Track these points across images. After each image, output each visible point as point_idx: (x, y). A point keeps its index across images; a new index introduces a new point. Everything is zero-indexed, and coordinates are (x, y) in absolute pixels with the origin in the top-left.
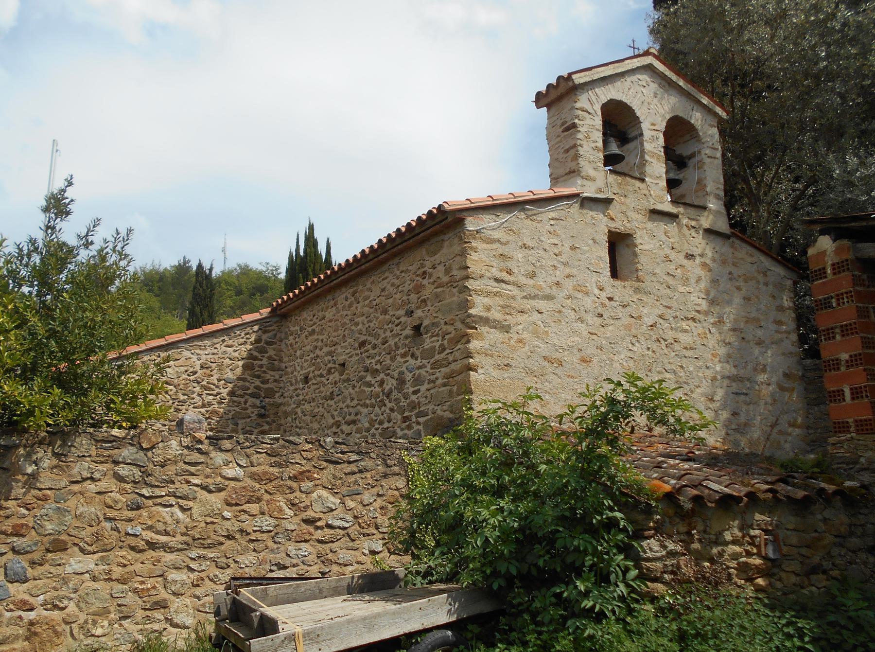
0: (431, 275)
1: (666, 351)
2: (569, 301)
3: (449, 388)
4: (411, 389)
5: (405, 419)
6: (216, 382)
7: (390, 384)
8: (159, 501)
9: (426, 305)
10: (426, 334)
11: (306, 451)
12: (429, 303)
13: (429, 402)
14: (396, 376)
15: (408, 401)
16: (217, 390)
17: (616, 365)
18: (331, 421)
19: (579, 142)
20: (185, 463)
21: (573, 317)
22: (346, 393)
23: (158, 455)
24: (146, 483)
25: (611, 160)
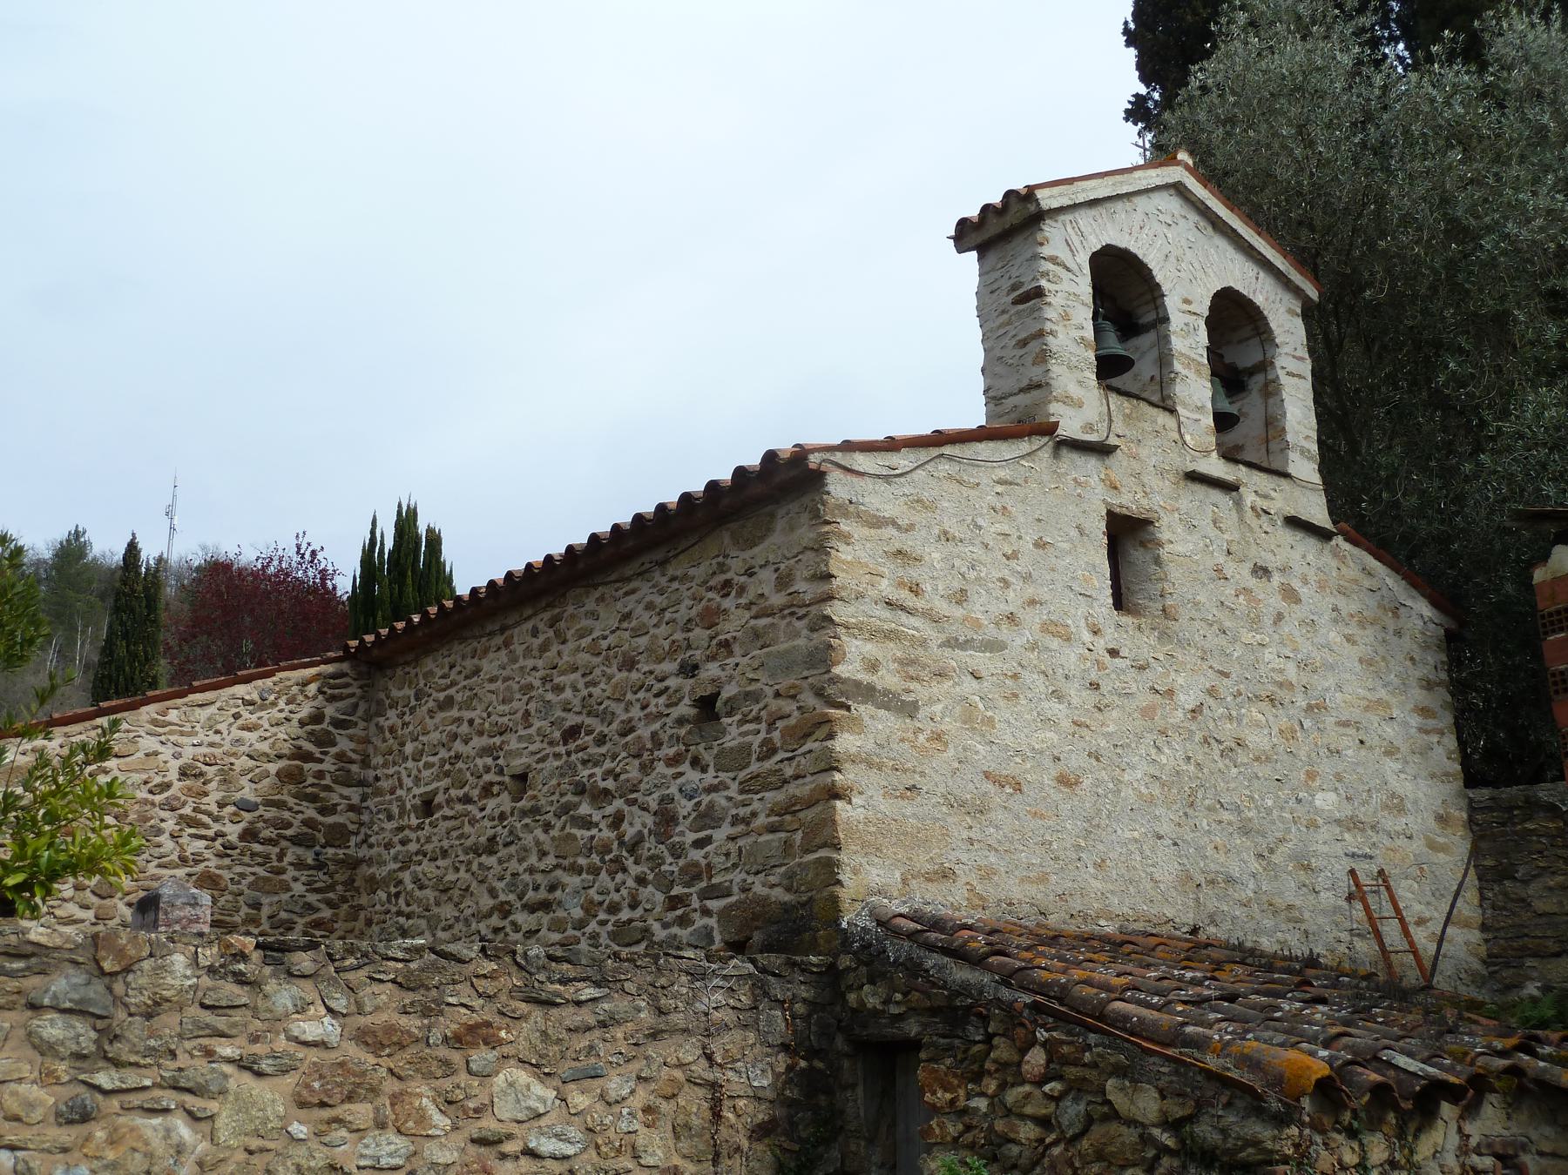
0: (742, 590)
1: (1220, 765)
2: (1033, 656)
3: (783, 835)
4: (691, 837)
5: (674, 902)
6: (214, 808)
7: (639, 823)
8: (135, 1099)
9: (731, 654)
10: (729, 714)
11: (485, 976)
12: (736, 648)
13: (735, 866)
14: (654, 806)
15: (681, 862)
16: (216, 827)
17: (1126, 792)
18: (487, 902)
19: (1048, 326)
20: (204, 1006)
21: (1043, 688)
22: (528, 840)
23: (140, 990)
24: (106, 1058)
25: (1110, 369)
